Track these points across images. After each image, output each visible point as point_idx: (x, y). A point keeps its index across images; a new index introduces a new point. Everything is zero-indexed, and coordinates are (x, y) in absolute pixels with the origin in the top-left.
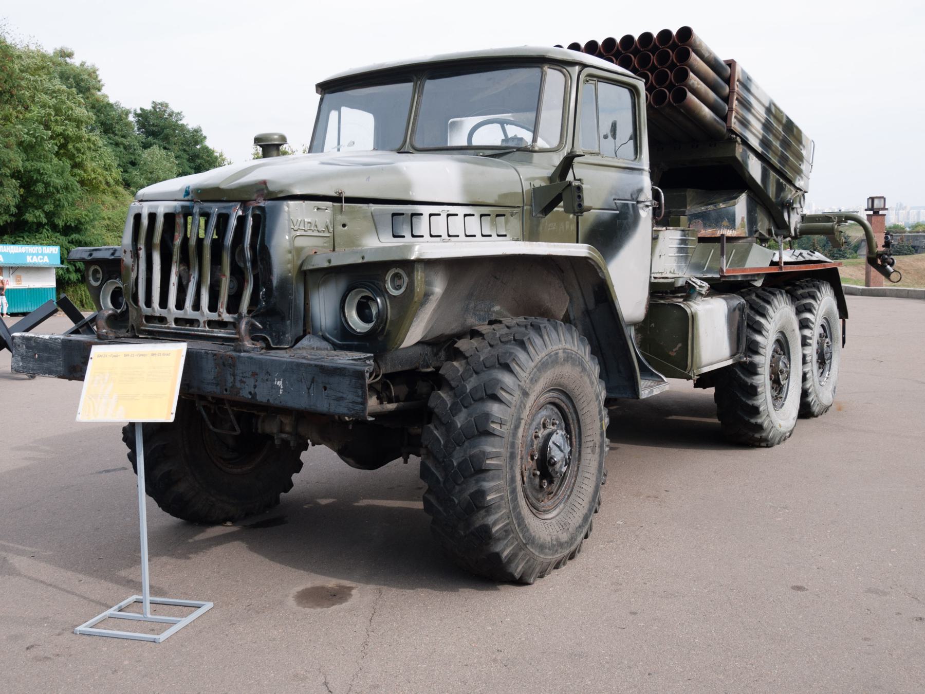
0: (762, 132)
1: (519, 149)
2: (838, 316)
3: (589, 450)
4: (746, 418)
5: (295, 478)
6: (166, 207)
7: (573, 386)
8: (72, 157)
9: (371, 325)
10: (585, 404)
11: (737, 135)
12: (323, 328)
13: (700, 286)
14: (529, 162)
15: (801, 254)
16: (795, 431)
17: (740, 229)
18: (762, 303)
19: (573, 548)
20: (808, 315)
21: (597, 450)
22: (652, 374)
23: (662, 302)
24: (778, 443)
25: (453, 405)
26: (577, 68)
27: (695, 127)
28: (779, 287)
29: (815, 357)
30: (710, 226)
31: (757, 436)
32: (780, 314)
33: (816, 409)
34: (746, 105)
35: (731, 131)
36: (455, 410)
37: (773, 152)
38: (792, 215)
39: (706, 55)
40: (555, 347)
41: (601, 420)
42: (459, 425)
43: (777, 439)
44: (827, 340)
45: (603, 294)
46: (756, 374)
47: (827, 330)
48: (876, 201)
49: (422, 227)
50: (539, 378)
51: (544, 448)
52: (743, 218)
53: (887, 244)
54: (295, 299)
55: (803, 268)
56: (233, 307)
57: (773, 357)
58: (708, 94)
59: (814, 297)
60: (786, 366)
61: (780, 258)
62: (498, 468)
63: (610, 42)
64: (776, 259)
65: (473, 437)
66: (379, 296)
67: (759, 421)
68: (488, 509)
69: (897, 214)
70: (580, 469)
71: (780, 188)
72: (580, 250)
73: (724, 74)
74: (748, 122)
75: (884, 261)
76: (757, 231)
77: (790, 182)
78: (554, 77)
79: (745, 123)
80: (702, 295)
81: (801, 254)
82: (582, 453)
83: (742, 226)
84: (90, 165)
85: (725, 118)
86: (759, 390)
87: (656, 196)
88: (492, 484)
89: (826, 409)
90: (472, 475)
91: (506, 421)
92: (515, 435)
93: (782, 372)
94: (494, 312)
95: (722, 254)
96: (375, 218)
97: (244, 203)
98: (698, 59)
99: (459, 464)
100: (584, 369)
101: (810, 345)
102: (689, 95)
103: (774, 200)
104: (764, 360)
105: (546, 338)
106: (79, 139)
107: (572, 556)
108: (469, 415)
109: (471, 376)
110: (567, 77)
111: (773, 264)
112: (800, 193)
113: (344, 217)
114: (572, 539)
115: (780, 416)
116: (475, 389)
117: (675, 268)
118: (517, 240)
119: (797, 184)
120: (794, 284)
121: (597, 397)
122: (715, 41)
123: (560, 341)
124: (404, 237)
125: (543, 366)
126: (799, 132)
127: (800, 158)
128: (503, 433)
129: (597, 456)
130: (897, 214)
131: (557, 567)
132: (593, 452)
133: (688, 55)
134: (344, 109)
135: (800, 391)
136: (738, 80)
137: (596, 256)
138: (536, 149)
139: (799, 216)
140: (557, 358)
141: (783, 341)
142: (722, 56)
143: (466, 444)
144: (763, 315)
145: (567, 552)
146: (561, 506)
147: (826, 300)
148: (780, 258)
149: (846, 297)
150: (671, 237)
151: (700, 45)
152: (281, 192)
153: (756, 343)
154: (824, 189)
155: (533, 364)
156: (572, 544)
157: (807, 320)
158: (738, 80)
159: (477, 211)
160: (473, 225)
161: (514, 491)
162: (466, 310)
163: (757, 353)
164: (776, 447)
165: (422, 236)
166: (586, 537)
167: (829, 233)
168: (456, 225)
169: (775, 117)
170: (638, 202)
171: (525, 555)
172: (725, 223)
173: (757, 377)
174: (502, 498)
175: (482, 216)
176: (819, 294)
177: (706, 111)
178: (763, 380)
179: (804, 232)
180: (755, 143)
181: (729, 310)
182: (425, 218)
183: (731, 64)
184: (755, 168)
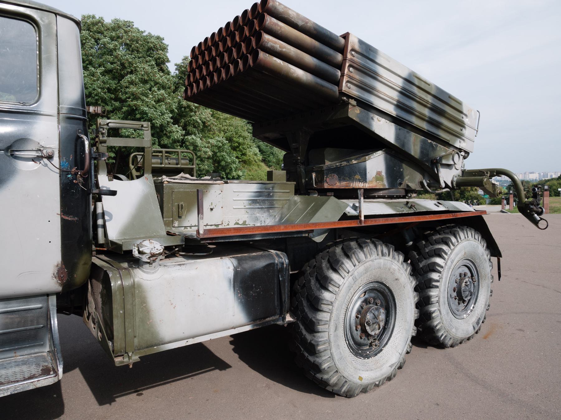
8: (241, 151)
30: (344, 180)
35: (342, 94)
39: (300, 23)
77: (447, 144)
79: (369, 89)
84: (248, 153)
85: (338, 83)
106: (244, 144)
111: (345, 217)
127: (462, 125)
136: (353, 50)
157: (435, 264)
164: (448, 350)
172: (357, 177)
176: (453, 239)
177: (299, 73)
184: (385, 130)
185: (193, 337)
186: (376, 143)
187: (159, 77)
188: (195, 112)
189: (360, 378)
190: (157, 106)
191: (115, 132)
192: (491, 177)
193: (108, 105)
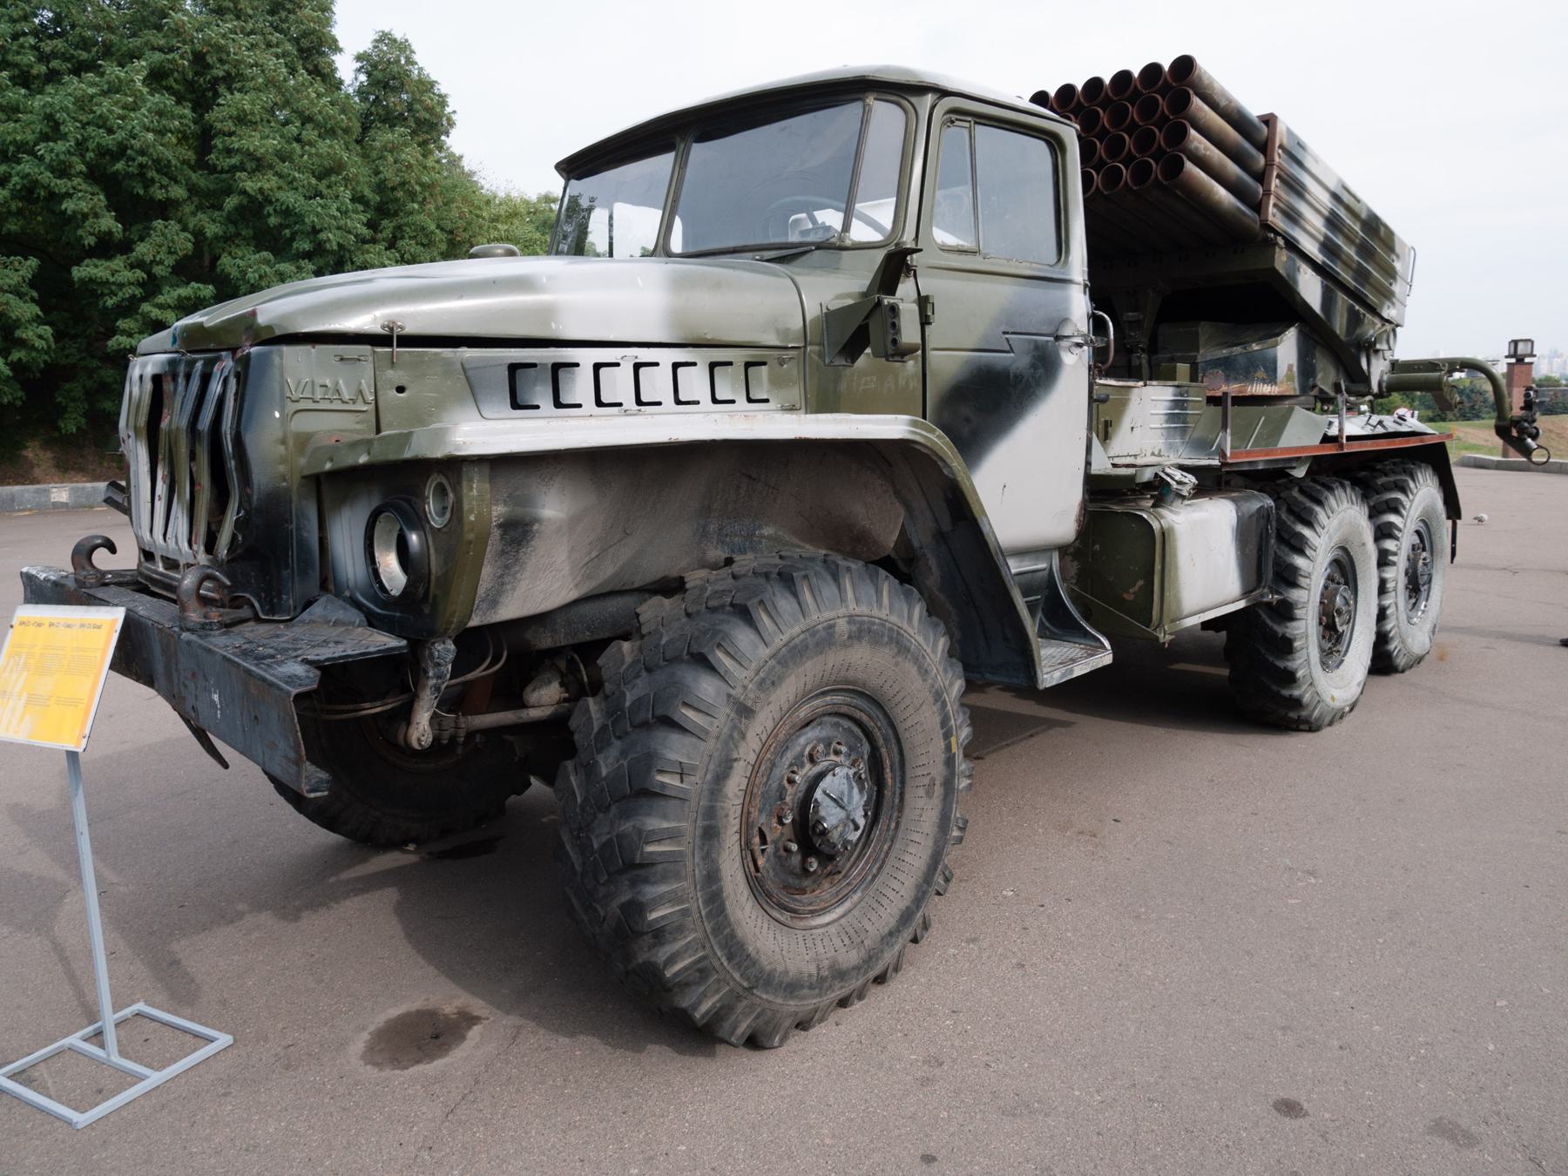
0: (1324, 230)
1: (820, 246)
2: (1444, 516)
3: (921, 792)
4: (1275, 688)
7: (881, 682)
11: (1277, 233)
12: (351, 583)
13: (1179, 483)
14: (835, 268)
15: (1380, 423)
18: (1309, 504)
20: (1393, 518)
21: (939, 790)
22: (1086, 634)
23: (1117, 508)
24: (1331, 724)
25: (604, 728)
26: (929, 98)
27: (1181, 217)
30: (1236, 380)
31: (1293, 715)
32: (1342, 519)
33: (1401, 661)
34: (1296, 188)
35: (1268, 227)
36: (602, 741)
37: (1345, 263)
38: (1373, 361)
39: (1223, 103)
40: (827, 615)
42: (604, 772)
43: (1327, 720)
44: (1424, 554)
46: (1292, 618)
47: (1425, 539)
48: (1521, 346)
49: (580, 387)
50: (781, 678)
51: (806, 802)
52: (1290, 367)
53: (1528, 405)
54: (298, 529)
55: (1384, 445)
57: (1326, 587)
58: (1224, 166)
59: (1404, 490)
60: (1347, 603)
61: (1341, 430)
62: (674, 858)
63: (1067, 91)
64: (1334, 431)
65: (624, 797)
66: (413, 528)
67: (1296, 693)
68: (659, 934)
69: (1551, 364)
70: (902, 827)
71: (1355, 320)
73: (1255, 139)
74: (1300, 214)
75: (1522, 431)
76: (1314, 386)
77: (1374, 311)
78: (885, 116)
79: (1293, 216)
80: (1183, 497)
81: (1380, 423)
82: (907, 796)
83: (1289, 378)
85: (1258, 207)
86: (1296, 644)
87: (1098, 326)
88: (662, 889)
89: (1420, 659)
90: (621, 872)
91: (694, 768)
93: (1339, 612)
94: (762, 536)
95: (1224, 427)
96: (470, 373)
98: (1206, 108)
99: (604, 846)
101: (1394, 564)
102: (1189, 165)
103: (1343, 337)
104: (1308, 598)
105: (807, 596)
108: (624, 753)
109: (638, 676)
110: (911, 115)
111: (1326, 439)
112: (1388, 327)
113: (400, 373)
115: (1336, 682)
116: (638, 703)
117: (1161, 446)
118: (792, 409)
119: (1386, 313)
120: (1372, 472)
121: (938, 696)
122: (1242, 78)
123: (843, 600)
124: (537, 407)
125: (794, 654)
127: (1391, 274)
129: (936, 801)
130: (1551, 364)
132: (929, 794)
133: (1187, 101)
135: (1373, 638)
136: (1281, 147)
137: (937, 439)
138: (848, 243)
139: (1387, 363)
140: (831, 635)
141: (1345, 560)
142: (1255, 109)
143: (614, 810)
144: (1309, 524)
146: (856, 897)
147: (1424, 493)
148: (1341, 430)
150: (1149, 404)
151: (1211, 85)
153: (1295, 570)
154: (1428, 322)
155: (765, 652)
156: (870, 968)
157: (1391, 524)
158: (1281, 147)
159: (703, 357)
160: (695, 382)
162: (704, 534)
163: (1294, 584)
164: (1326, 731)
165: (579, 406)
166: (843, 1003)
167: (1435, 387)
170: (1058, 338)
171: (752, 1007)
172: (1261, 373)
173: (1294, 624)
174: (685, 913)
175: (713, 366)
176: (1412, 485)
177: (1222, 193)
178: (1306, 629)
180: (1311, 247)
181: (1239, 519)
182: (627, 371)
183: (1269, 120)
184: (1310, 288)
185: (1203, 611)
186: (1286, 309)
187: (313, 97)
188: (423, 203)
189: (1333, 699)
190: (322, 187)
191: (40, 337)
192: (1450, 372)
193: (176, 182)
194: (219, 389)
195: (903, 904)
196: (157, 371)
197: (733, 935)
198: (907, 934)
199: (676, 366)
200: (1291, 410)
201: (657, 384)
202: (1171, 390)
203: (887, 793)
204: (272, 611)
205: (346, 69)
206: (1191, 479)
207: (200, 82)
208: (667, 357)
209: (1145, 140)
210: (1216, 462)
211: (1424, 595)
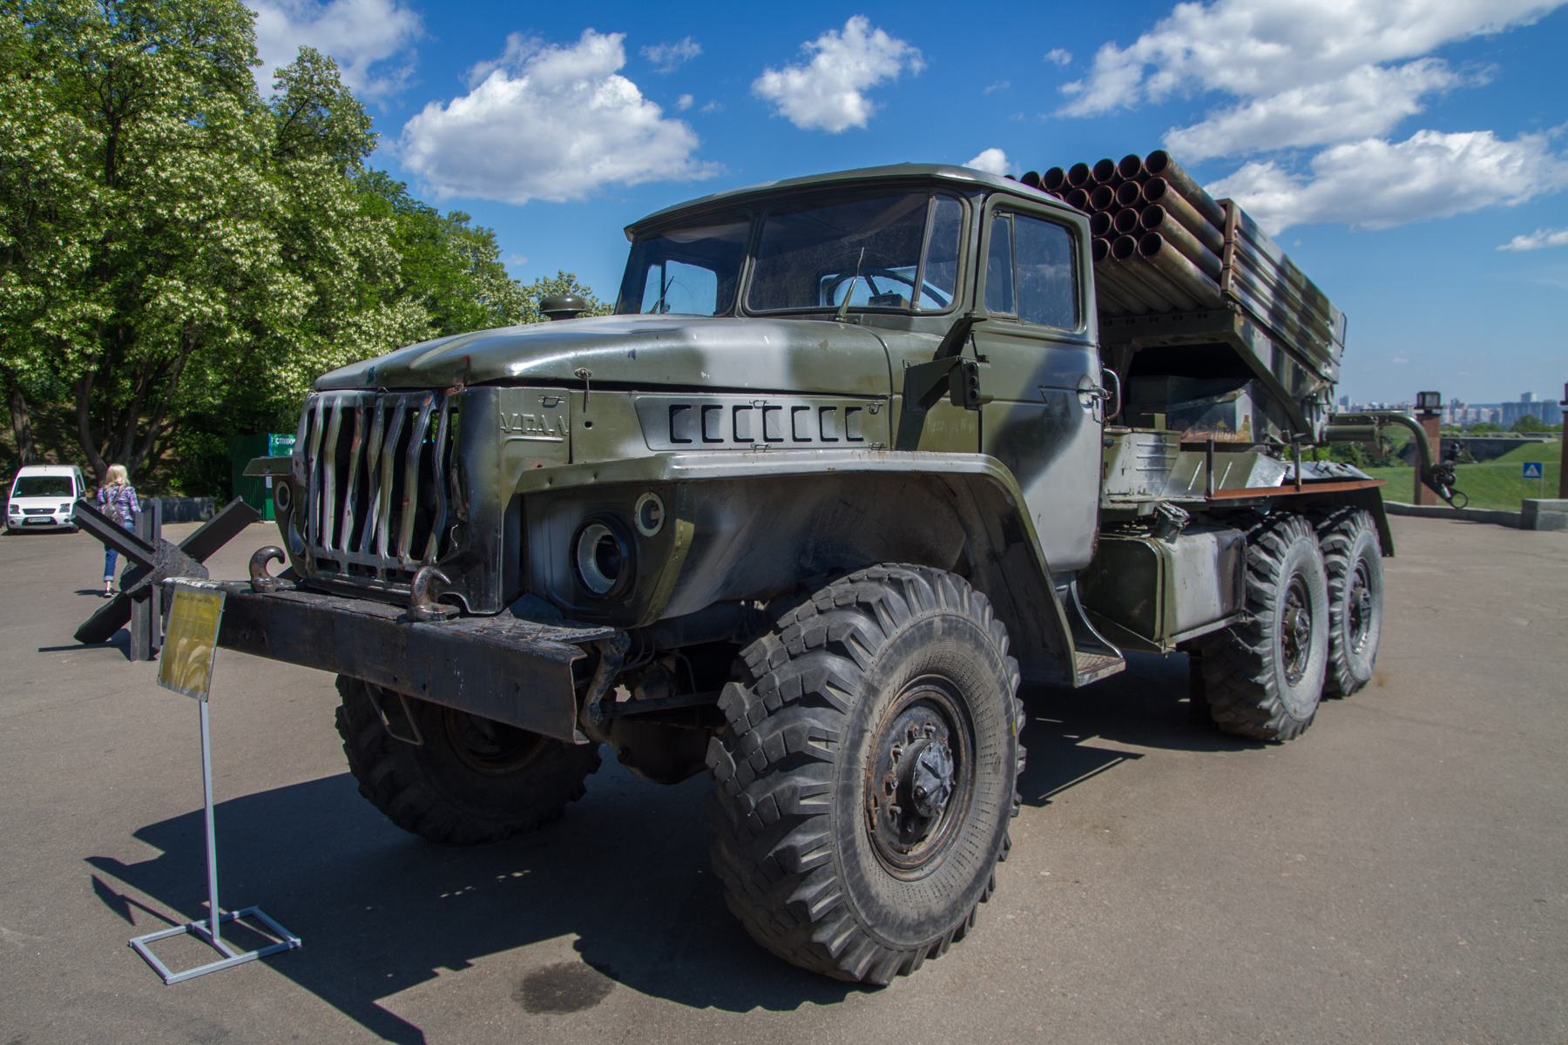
3: (989, 769)
5: (589, 781)
6: (345, 398)
9: (612, 582)
10: (983, 698)
12: (549, 583)
16: (1316, 718)
17: (1243, 431)
19: (956, 924)
20: (1336, 558)
21: (1003, 767)
28: (1295, 513)
29: (1347, 614)
30: (1200, 428)
35: (1227, 296)
40: (928, 613)
41: (1010, 721)
45: (1015, 529)
48: (1428, 398)
49: (724, 428)
52: (1246, 418)
56: (418, 552)
57: (1286, 610)
61: (1297, 473)
62: (819, 812)
69: (1452, 413)
72: (974, 463)
74: (1252, 285)
77: (1313, 369)
79: (1247, 287)
83: (1246, 428)
85: (1218, 278)
87: (1107, 381)
89: (1360, 685)
91: (836, 735)
92: (852, 759)
97: (440, 393)
100: (979, 645)
103: (1290, 393)
104: (1273, 619)
107: (959, 935)
114: (953, 909)
115: (1296, 691)
118: (881, 448)
120: (1320, 509)
121: (1003, 686)
126: (1325, 301)
128: (830, 755)
131: (932, 954)
132: (996, 771)
134: (670, 264)
137: (1001, 472)
141: (1300, 587)
145: (947, 929)
147: (1363, 533)
148: (1297, 473)
149: (1388, 516)
150: (1138, 446)
152: (488, 372)
155: (885, 643)
156: (952, 918)
160: (809, 423)
161: (849, 847)
168: (781, 424)
169: (1291, 280)
172: (1221, 424)
175: (822, 410)
177: (1191, 266)
178: (1271, 647)
179: (1330, 438)
180: (1262, 313)
182: (785, 414)
184: (1262, 347)
194: (427, 421)
195: (979, 864)
196: (346, 404)
197: (862, 877)
198: (979, 894)
199: (794, 409)
200: (1255, 457)
201: (781, 424)
202: (1152, 437)
203: (963, 769)
204: (479, 607)
205: (266, 83)
206: (1183, 513)
207: (118, 97)
208: (787, 402)
209: (1127, 222)
210: (1202, 499)
211: (1363, 626)
